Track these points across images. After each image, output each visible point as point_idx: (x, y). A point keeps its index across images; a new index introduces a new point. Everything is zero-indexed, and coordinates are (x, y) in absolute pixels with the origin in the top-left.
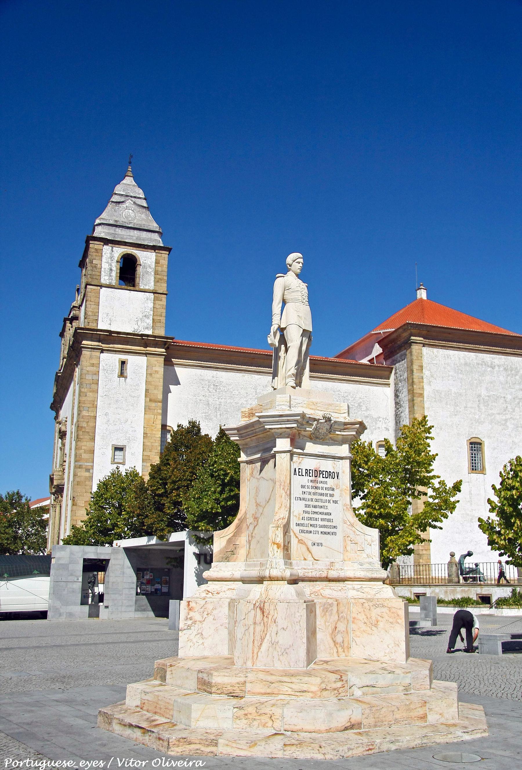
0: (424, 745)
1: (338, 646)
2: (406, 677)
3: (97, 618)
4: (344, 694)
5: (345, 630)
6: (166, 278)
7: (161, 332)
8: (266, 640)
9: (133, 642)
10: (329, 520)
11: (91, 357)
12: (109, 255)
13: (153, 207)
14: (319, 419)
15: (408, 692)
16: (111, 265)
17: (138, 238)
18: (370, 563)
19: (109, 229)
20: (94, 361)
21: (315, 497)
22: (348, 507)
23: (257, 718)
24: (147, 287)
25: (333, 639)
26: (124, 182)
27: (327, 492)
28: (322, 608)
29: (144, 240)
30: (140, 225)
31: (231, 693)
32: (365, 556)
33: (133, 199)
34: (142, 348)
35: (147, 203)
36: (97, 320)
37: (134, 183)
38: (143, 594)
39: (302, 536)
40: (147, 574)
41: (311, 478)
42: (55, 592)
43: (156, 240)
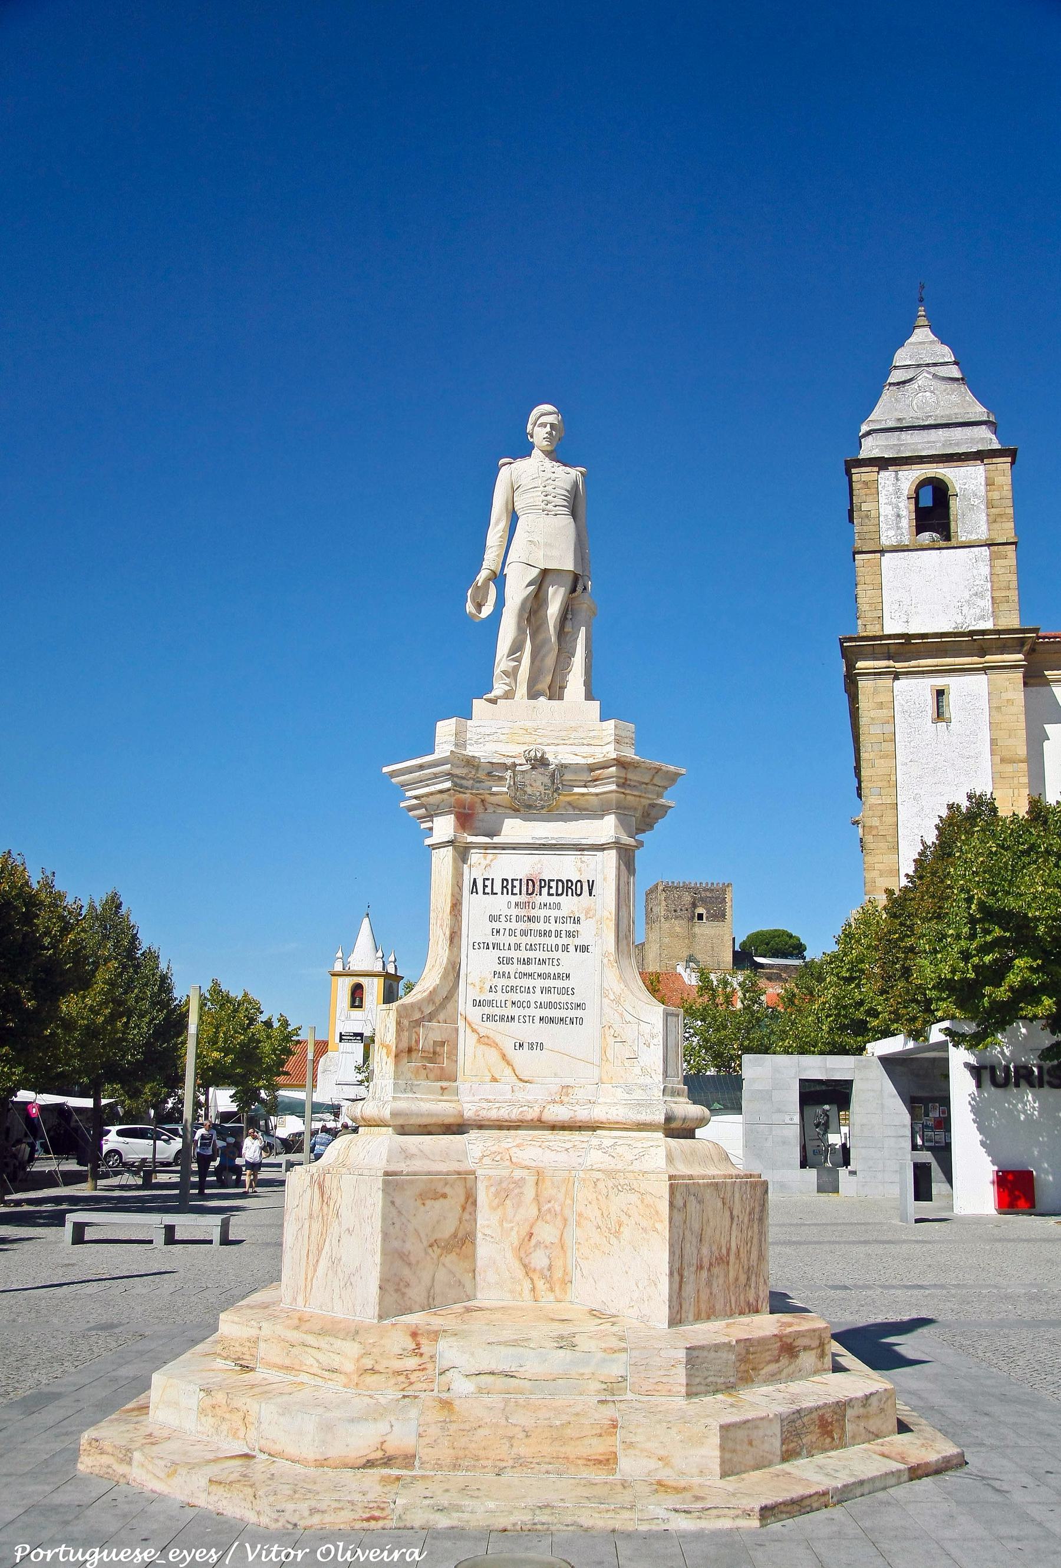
0: (539, 1527)
1: (535, 1277)
2: (613, 1361)
3: (836, 1195)
4: (424, 1386)
5: (556, 1241)
6: (1010, 511)
7: (1012, 620)
8: (324, 1252)
9: (904, 1242)
10: (565, 991)
11: (876, 691)
12: (891, 489)
13: (973, 376)
14: (515, 765)
15: (616, 1398)
16: (897, 507)
17: (947, 443)
18: (644, 1088)
19: (887, 439)
20: (884, 698)
21: (524, 940)
22: (612, 959)
23: (227, 1416)
24: (973, 537)
25: (521, 1259)
26: (912, 340)
27: (560, 927)
28: (493, 1189)
29: (957, 445)
30: (948, 416)
31: (239, 1359)
32: (637, 1070)
33: (932, 369)
34: (976, 659)
35: (962, 370)
36: (881, 618)
37: (932, 337)
38: (928, 1149)
39: (489, 1028)
40: (934, 1108)
41: (515, 899)
42: (752, 1142)
43: (985, 438)
